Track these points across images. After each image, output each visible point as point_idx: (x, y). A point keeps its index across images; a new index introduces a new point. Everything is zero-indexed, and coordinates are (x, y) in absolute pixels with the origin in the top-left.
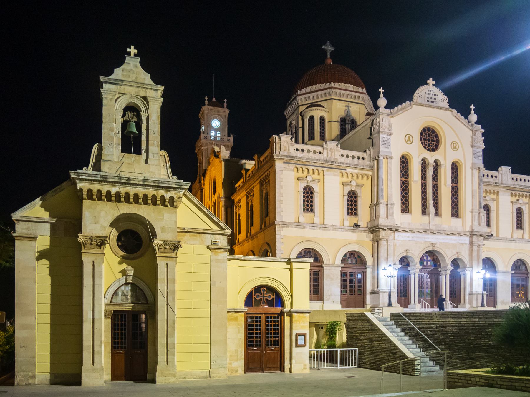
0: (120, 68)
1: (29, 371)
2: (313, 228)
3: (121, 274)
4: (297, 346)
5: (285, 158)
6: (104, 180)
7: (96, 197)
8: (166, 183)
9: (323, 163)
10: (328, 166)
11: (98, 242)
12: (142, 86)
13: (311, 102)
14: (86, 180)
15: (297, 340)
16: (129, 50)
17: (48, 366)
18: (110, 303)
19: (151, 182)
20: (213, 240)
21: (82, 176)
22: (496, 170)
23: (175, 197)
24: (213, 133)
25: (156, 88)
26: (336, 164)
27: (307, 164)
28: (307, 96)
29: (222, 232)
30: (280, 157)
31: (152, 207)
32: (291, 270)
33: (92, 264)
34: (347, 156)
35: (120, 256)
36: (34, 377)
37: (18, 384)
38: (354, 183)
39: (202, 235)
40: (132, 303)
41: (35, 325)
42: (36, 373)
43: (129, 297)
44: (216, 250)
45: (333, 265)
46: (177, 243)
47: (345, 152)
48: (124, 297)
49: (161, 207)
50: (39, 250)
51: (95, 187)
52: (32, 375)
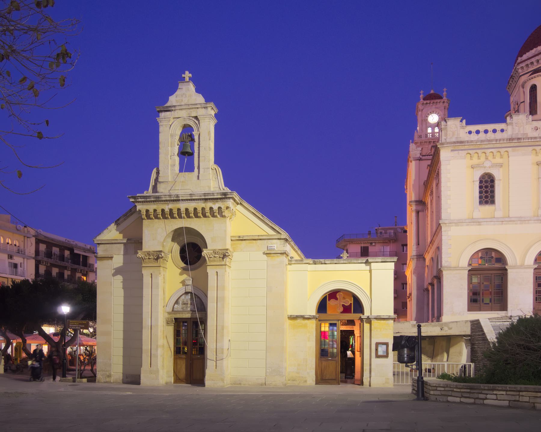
0: (175, 94)
1: (106, 371)
2: (492, 223)
3: (182, 284)
4: (378, 356)
5: (453, 145)
6: (158, 200)
7: (154, 216)
8: (211, 195)
9: (505, 142)
10: (515, 145)
11: (155, 256)
12: (192, 107)
13: (535, 68)
14: (143, 202)
15: (377, 350)
16: (183, 76)
17: (121, 366)
18: (172, 311)
19: (198, 196)
20: (269, 246)
21: (138, 199)
22: (504, 121)
23: (222, 207)
24: (430, 130)
25: (205, 106)
26: (524, 141)
27: (483, 147)
28: (528, 62)
29: (278, 236)
30: (445, 146)
31: (203, 219)
32: (370, 271)
33: (151, 276)
34: (486, 132)
35: (181, 268)
36: (109, 376)
37: (98, 382)
38: (487, 164)
39: (259, 241)
40: (191, 311)
41: (112, 331)
42: (112, 373)
43: (189, 305)
44: (272, 255)
45: (522, 266)
46: (225, 251)
47: (473, 128)
48: (185, 305)
49: (212, 218)
50: (114, 268)
51: (151, 207)
52: (108, 374)
